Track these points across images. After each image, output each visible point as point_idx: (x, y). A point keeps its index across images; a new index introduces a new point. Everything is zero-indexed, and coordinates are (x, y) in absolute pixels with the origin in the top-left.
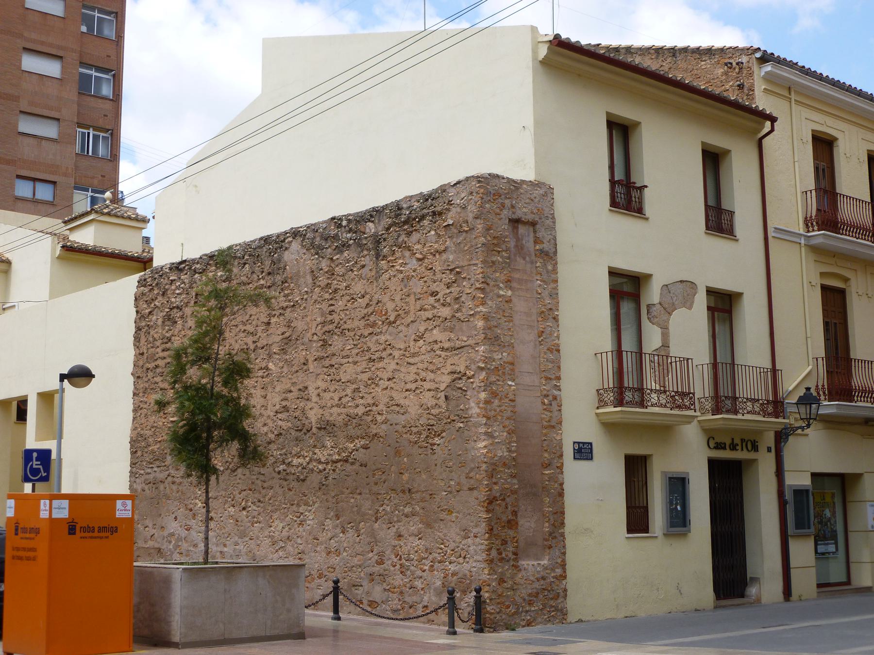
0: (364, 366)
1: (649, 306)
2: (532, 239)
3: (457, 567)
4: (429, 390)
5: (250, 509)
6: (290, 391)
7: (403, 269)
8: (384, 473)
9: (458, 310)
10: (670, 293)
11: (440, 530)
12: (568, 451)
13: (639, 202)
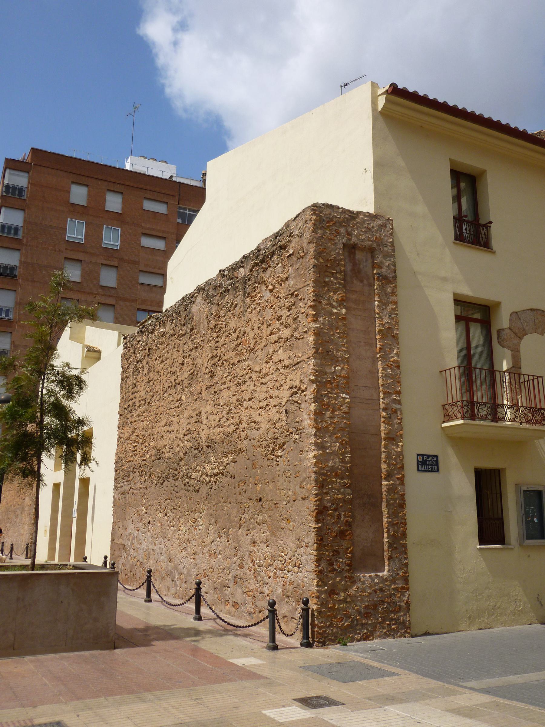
0: (234, 390)
1: (499, 332)
2: (369, 265)
3: (293, 576)
4: (275, 406)
5: (169, 515)
6: (192, 417)
7: (261, 301)
8: (245, 484)
9: (296, 330)
10: (520, 319)
11: (281, 539)
12: (411, 463)
13: (486, 238)
